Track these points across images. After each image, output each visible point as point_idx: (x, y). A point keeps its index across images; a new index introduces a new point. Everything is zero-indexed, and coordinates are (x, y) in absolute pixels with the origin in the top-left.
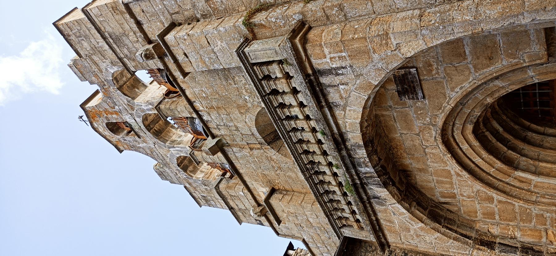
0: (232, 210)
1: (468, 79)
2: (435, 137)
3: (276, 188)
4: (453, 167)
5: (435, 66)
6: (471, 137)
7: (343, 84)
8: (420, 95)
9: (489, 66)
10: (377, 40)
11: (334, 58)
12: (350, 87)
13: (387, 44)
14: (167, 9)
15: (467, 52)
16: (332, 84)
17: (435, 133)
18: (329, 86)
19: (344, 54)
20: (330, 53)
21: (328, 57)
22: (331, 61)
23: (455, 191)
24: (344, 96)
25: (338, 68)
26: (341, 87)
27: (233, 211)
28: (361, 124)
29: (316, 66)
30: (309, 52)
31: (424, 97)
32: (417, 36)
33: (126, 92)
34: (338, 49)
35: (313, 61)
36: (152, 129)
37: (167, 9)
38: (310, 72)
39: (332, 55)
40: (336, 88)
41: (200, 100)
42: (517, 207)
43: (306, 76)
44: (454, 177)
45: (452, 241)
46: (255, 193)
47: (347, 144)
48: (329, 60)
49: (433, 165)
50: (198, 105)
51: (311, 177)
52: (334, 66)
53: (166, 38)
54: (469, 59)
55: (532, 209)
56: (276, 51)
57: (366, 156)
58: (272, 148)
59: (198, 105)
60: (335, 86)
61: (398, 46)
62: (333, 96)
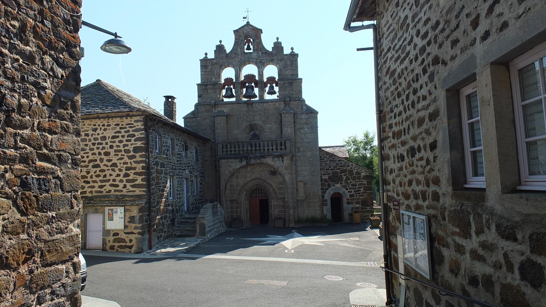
44: (245, 179)
61: (287, 176)
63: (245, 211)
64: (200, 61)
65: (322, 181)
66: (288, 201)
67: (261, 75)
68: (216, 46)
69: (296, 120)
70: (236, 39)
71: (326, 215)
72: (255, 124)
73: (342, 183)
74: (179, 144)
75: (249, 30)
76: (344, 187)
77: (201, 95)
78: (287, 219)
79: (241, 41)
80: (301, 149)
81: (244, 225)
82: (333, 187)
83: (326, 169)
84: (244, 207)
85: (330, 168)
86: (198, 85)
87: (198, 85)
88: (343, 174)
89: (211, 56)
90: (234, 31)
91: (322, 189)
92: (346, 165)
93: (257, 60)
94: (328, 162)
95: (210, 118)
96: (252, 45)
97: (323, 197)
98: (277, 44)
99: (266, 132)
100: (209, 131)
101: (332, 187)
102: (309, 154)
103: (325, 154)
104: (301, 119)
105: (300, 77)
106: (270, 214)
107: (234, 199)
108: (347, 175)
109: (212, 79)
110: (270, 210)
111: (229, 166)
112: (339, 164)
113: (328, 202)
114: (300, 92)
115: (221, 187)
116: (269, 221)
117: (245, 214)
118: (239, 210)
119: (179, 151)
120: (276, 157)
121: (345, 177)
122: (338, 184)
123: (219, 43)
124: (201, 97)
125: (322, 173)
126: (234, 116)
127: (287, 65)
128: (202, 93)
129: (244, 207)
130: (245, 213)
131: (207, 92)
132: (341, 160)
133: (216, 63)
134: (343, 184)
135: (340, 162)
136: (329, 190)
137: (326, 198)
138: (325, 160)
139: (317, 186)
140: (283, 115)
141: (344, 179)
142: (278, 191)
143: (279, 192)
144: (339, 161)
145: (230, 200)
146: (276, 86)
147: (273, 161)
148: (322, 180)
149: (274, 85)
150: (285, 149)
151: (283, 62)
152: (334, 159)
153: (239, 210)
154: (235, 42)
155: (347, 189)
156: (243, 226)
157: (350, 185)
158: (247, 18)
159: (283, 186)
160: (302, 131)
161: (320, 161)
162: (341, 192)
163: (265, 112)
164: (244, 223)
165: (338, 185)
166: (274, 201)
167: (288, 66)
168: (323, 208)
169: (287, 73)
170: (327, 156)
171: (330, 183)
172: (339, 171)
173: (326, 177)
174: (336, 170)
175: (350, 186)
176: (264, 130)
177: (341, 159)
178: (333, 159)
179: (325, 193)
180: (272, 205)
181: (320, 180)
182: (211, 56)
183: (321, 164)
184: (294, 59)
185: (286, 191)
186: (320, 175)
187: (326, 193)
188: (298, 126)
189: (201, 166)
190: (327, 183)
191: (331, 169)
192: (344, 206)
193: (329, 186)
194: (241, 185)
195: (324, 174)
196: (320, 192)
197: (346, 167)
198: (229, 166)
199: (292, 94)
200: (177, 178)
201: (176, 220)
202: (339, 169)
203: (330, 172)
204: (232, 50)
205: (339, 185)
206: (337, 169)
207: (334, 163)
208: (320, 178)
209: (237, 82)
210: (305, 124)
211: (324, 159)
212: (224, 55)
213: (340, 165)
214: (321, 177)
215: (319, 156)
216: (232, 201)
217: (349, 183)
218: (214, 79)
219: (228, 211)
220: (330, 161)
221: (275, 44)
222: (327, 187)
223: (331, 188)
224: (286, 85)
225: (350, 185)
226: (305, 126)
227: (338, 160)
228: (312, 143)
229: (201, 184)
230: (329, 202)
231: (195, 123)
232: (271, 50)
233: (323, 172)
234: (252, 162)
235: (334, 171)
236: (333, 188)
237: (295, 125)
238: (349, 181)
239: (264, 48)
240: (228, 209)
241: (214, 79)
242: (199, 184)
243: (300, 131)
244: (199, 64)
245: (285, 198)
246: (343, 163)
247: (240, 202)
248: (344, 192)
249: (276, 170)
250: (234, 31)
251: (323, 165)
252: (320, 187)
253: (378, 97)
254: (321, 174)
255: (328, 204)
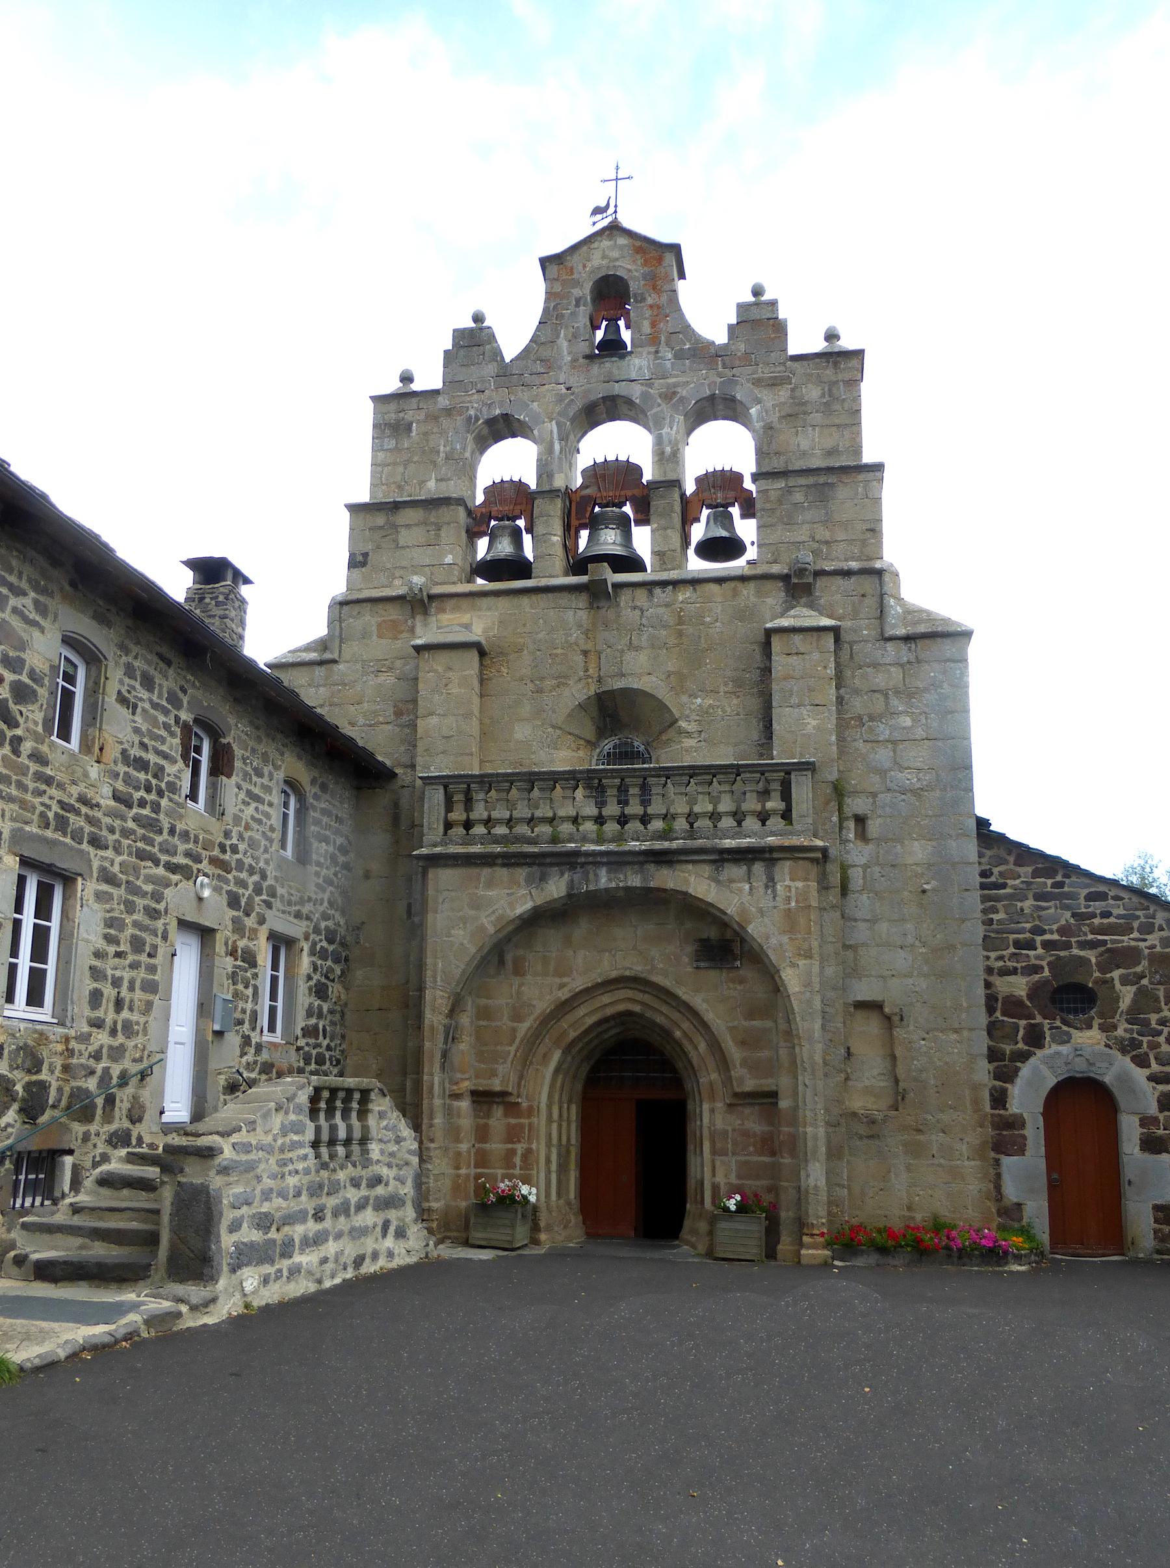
0: (392, 506)
1: (718, 1018)
2: (631, 969)
3: (487, 662)
4: (579, 983)
5: (738, 987)
6: (621, 1007)
7: (751, 889)
8: (702, 964)
9: (733, 1041)
10: (806, 946)
11: (790, 891)
12: (746, 898)
13: (800, 955)
14: (860, 642)
15: (754, 1022)
16: (752, 876)
17: (637, 967)
18: (749, 871)
19: (793, 904)
20: (797, 888)
21: (791, 884)
22: (786, 886)
23: (529, 977)
24: (734, 885)
25: (774, 891)
26: (747, 887)
27: (388, 506)
28: (686, 894)
29: (780, 864)
30: (801, 862)
31: (697, 968)
32: (805, 987)
33: (700, 403)
34: (801, 898)
35: (788, 863)
36: (604, 403)
37: (860, 642)
38: (775, 855)
39: (793, 890)
40: (746, 878)
41: (698, 605)
42: (507, 1048)
43: (772, 849)
44: (558, 980)
45: (463, 967)
46: (465, 603)
47: (652, 865)
48: (786, 883)
49: (580, 958)
50: (688, 594)
51: (574, 779)
52: (779, 887)
53: (832, 634)
54: (744, 1023)
55: (505, 1066)
56: (804, 816)
57: (629, 884)
58: (589, 698)
59: (688, 594)
60: (749, 878)
61: (793, 965)
62: (736, 871)
63: (554, 1158)
64: (371, 405)
65: (991, 1010)
66: (796, 1108)
67: (668, 456)
68: (454, 331)
69: (848, 673)
70: (549, 295)
71: (1019, 1205)
72: (626, 692)
73: (1115, 1027)
74: (147, 706)
75: (615, 254)
76: (1128, 1047)
77: (365, 555)
78: (785, 1215)
79: (577, 305)
80: (874, 827)
81: (543, 1237)
82: (1055, 1048)
83: (1018, 944)
84: (549, 1136)
85: (1038, 939)
86: (355, 509)
87: (355, 509)
88: (1116, 974)
89: (430, 377)
90: (546, 263)
91: (993, 1055)
92: (1136, 924)
93: (650, 386)
94: (1028, 904)
95: (398, 663)
96: (628, 327)
97: (999, 1099)
98: (754, 309)
99: (681, 732)
100: (390, 727)
101: (1051, 1049)
102: (918, 852)
103: (1011, 859)
104: (875, 665)
105: (868, 458)
106: (691, 1184)
107: (496, 1085)
108: (1145, 982)
109: (422, 483)
110: (693, 1161)
111: (476, 904)
112: (1094, 916)
113: (1029, 1132)
114: (874, 530)
115: (428, 1015)
116: (687, 1224)
117: (554, 1177)
118: (520, 1148)
119: (143, 746)
120: (736, 861)
121: (1127, 996)
122: (1090, 1027)
123: (471, 324)
124: (363, 564)
125: (991, 963)
126: (521, 650)
127: (804, 404)
128: (369, 547)
129: (549, 1136)
130: (554, 1167)
131: (396, 541)
132: (1102, 896)
133: (448, 412)
134: (1120, 1032)
135: (1097, 906)
136: (1032, 1060)
137: (1015, 1106)
138: (1008, 890)
139: (965, 1033)
140: (777, 644)
141: (1125, 1002)
142: (735, 1053)
143: (744, 1063)
144: (1090, 897)
145: (474, 1093)
146: (747, 513)
147: (718, 882)
148: (991, 1002)
149: (735, 511)
150: (787, 815)
151: (784, 393)
152: (1060, 885)
153: (520, 1148)
154: (546, 311)
155: (1142, 1062)
156: (535, 1242)
157: (1162, 1039)
158: (611, 210)
159: (768, 1024)
160: (883, 731)
161: (985, 899)
162: (1107, 1079)
163: (680, 634)
164: (542, 1224)
165: (1089, 1033)
166: (712, 1111)
167: (809, 408)
168: (997, 1162)
169: (805, 444)
170: (1021, 870)
171: (1038, 1019)
172: (1092, 956)
173: (1019, 986)
174: (1075, 951)
175: (1158, 1045)
176: (676, 721)
177: (1102, 888)
178: (1055, 885)
179: (1005, 1074)
180: (706, 1132)
181: (983, 1001)
182: (430, 377)
183: (985, 911)
184: (840, 377)
185: (783, 1052)
186: (983, 975)
187: (1018, 1081)
188: (858, 705)
189: (326, 896)
190: (1023, 1023)
191: (1047, 945)
192: (1125, 1159)
193: (1035, 1039)
194: (538, 1012)
195: (1005, 972)
196: (983, 1072)
197: (1135, 935)
198: (476, 904)
199: (827, 543)
200: (99, 896)
201: (68, 1160)
202: (1092, 945)
203: (1038, 957)
204: (526, 350)
205: (1090, 1038)
206: (1083, 945)
207: (1067, 907)
208: (980, 991)
209: (547, 488)
210: (897, 692)
211: (1004, 886)
212: (491, 369)
213: (1097, 921)
214: (988, 985)
215: (977, 869)
216: (483, 1098)
217: (1154, 1025)
218: (432, 484)
219: (459, 1154)
220: (1038, 897)
221: (742, 308)
222: (1021, 1045)
223: (1047, 1051)
224: (798, 497)
225: (1162, 1039)
226: (897, 704)
227: (1084, 892)
228: (938, 793)
229: (320, 992)
230: (1034, 1133)
231: (322, 689)
232: (720, 337)
233: (1001, 958)
234: (597, 881)
235: (1062, 953)
236: (1058, 1053)
237: (840, 700)
238: (1154, 1018)
239: (687, 329)
240: (458, 1140)
241: (432, 484)
242: (302, 987)
243: (871, 729)
244: (366, 414)
245: (774, 1095)
246: (1115, 912)
247: (530, 1109)
248: (1124, 1079)
249: (729, 935)
250: (546, 263)
251: (995, 917)
252: (982, 1043)
253: (1076, 869)
254: (989, 970)
255: (1030, 1143)
